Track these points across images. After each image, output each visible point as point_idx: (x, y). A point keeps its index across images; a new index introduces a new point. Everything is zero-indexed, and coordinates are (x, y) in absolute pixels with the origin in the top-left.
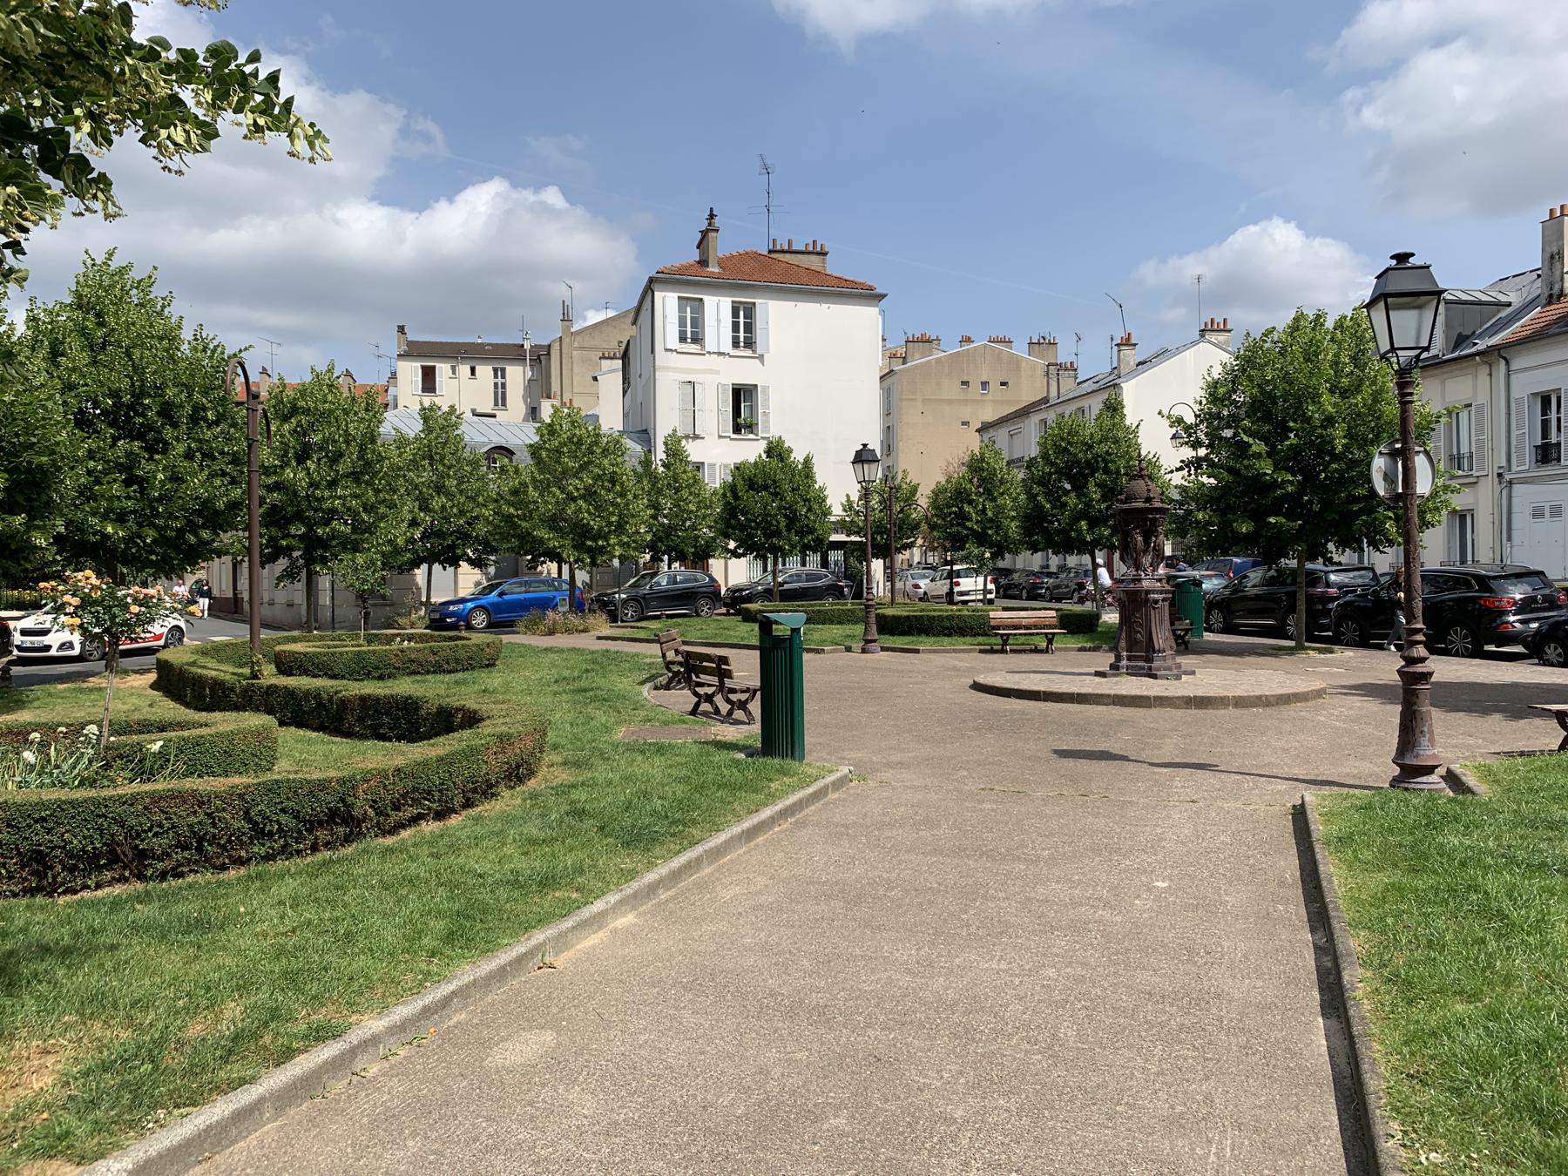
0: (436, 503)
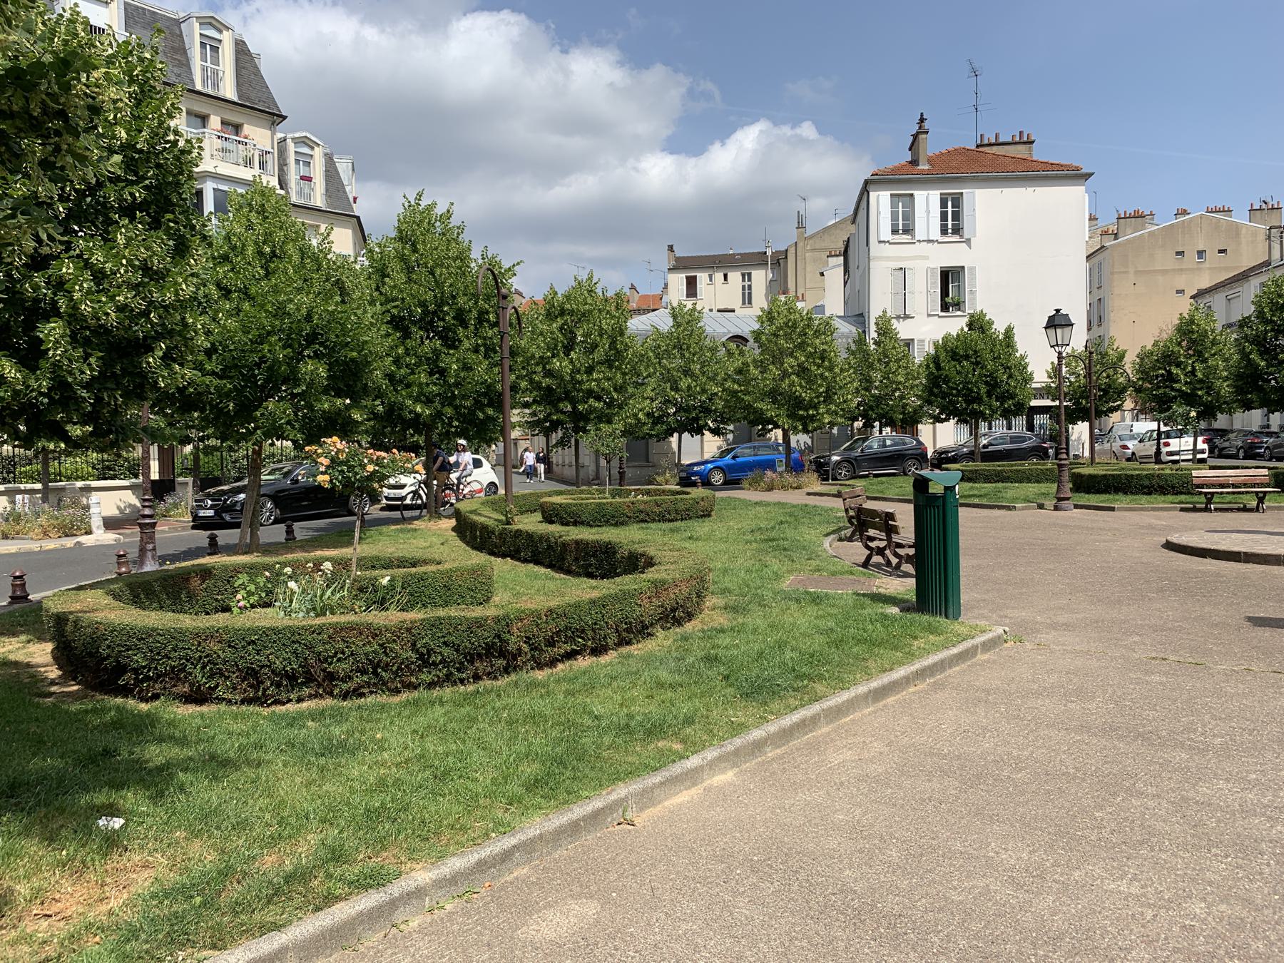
0: (683, 384)
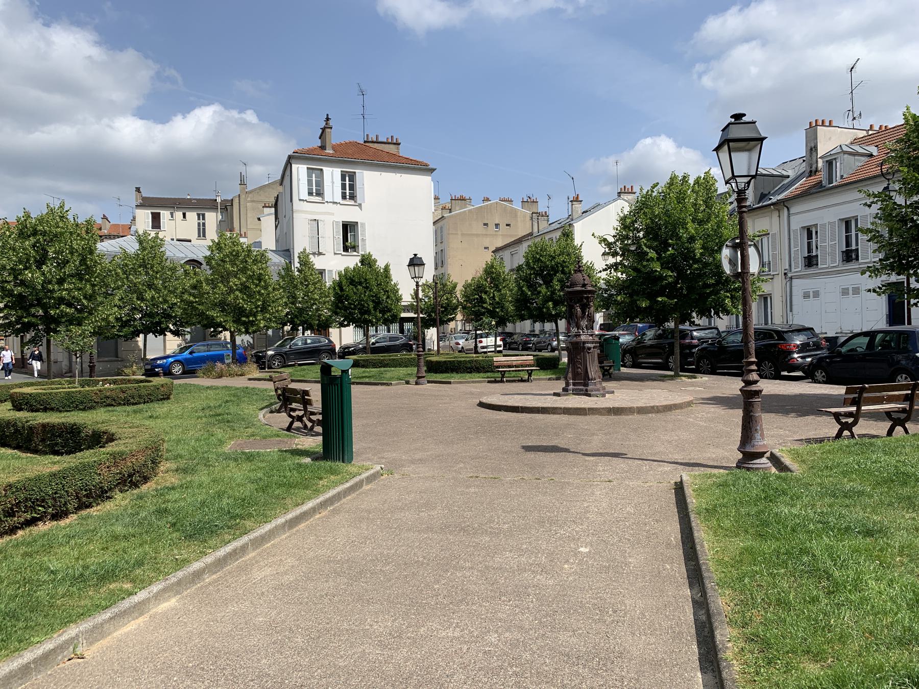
0: (148, 295)
